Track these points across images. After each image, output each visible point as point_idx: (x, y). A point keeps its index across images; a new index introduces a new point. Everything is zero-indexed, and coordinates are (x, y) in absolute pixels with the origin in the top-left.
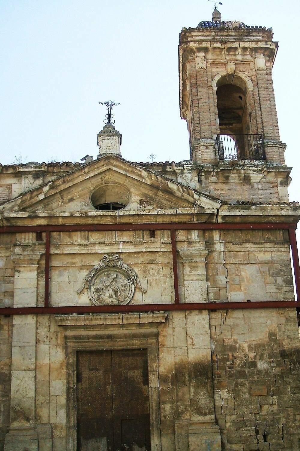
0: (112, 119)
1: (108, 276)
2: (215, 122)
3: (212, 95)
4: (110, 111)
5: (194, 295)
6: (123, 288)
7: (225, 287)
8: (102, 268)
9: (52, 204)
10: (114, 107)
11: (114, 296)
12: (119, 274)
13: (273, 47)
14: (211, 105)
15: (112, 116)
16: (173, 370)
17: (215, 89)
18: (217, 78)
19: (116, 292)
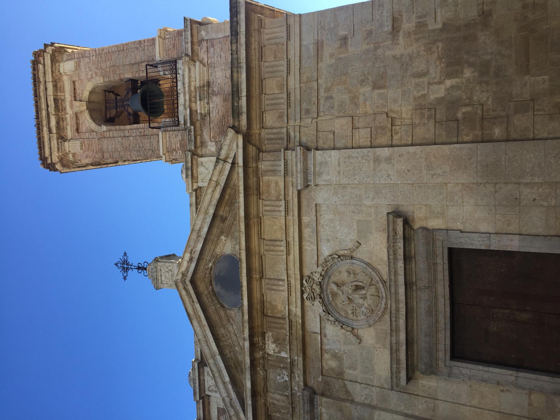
0: (143, 265)
1: (335, 295)
2: (105, 141)
3: (111, 133)
4: (134, 267)
5: (362, 169)
6: (352, 275)
7: (336, 146)
8: (323, 303)
9: (238, 362)
10: (130, 261)
11: (363, 292)
12: (331, 280)
13: (50, 49)
14: (122, 135)
15: (139, 265)
16: (426, 87)
17: (104, 128)
18: (93, 126)
19: (358, 288)
